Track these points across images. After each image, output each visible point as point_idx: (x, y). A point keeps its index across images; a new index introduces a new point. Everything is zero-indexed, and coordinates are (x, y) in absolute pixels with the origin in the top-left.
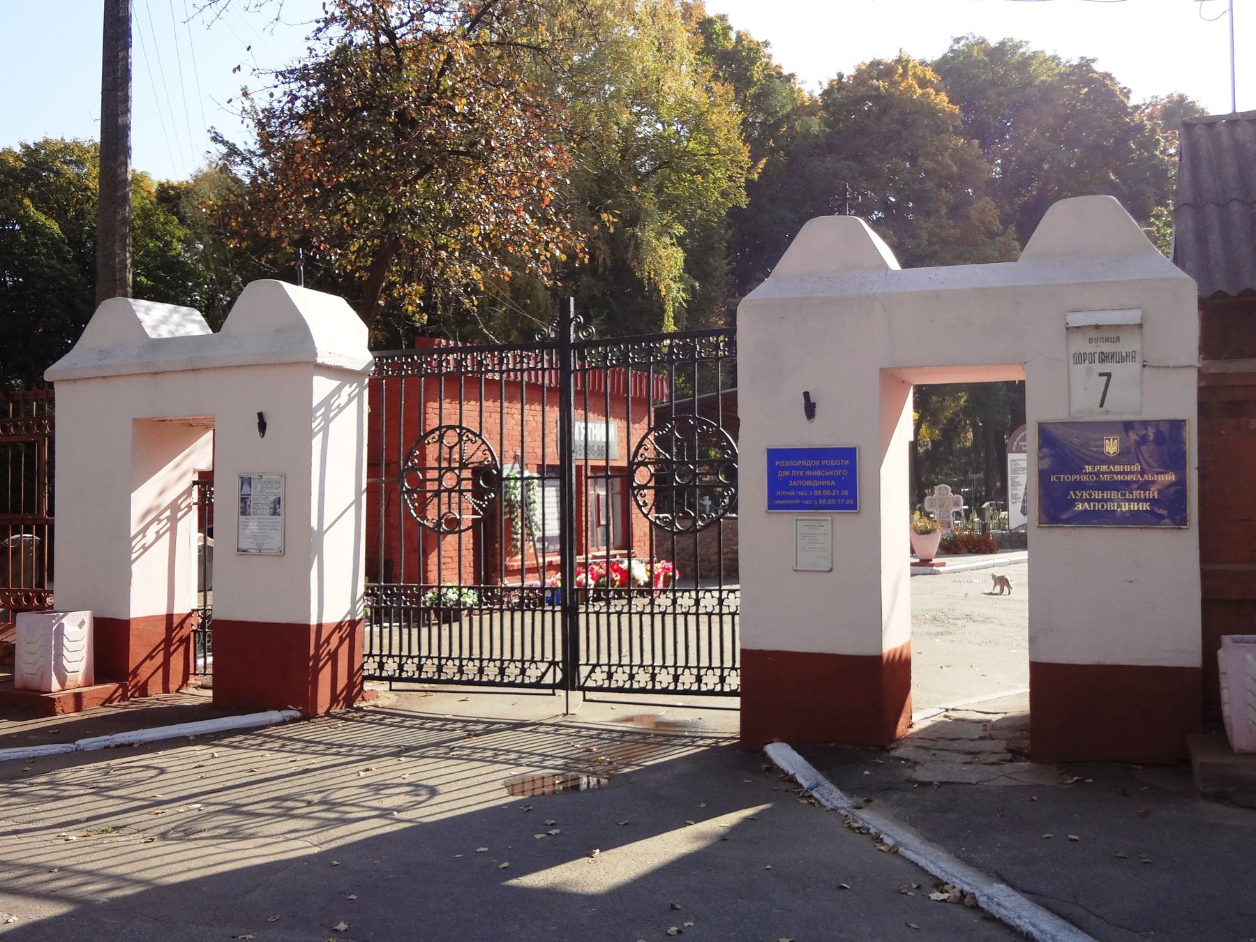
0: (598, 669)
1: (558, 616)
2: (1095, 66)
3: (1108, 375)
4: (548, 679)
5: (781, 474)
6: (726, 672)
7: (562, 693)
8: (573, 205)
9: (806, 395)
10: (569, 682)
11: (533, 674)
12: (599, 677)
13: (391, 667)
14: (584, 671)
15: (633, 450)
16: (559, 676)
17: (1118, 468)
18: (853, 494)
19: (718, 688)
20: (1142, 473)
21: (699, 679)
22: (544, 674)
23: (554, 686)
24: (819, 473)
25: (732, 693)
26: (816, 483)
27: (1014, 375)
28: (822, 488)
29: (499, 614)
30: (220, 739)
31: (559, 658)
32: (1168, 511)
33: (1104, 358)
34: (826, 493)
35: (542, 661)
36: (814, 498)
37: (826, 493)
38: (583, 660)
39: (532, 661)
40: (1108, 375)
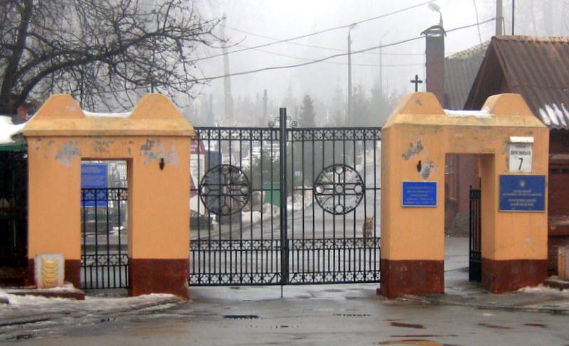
0: (298, 275)
1: (279, 253)
2: (453, 46)
3: (522, 159)
4: (274, 281)
5: (408, 192)
6: (356, 273)
7: (280, 286)
8: (124, 55)
9: (420, 162)
10: (284, 282)
11: (267, 279)
12: (298, 278)
13: (349, 277)
14: (291, 276)
15: (315, 178)
16: (279, 279)
17: (524, 191)
18: (435, 200)
19: (363, 280)
20: (531, 193)
21: (355, 276)
22: (272, 279)
23: (277, 284)
24: (422, 192)
25: (378, 282)
26: (421, 196)
27: (444, 156)
28: (423, 197)
29: (332, 251)
30: (464, 302)
31: (279, 271)
32: (538, 207)
33: (521, 153)
34: (425, 199)
35: (272, 273)
36: (420, 201)
37: (425, 199)
38: (290, 271)
39: (267, 273)
40: (522, 159)
